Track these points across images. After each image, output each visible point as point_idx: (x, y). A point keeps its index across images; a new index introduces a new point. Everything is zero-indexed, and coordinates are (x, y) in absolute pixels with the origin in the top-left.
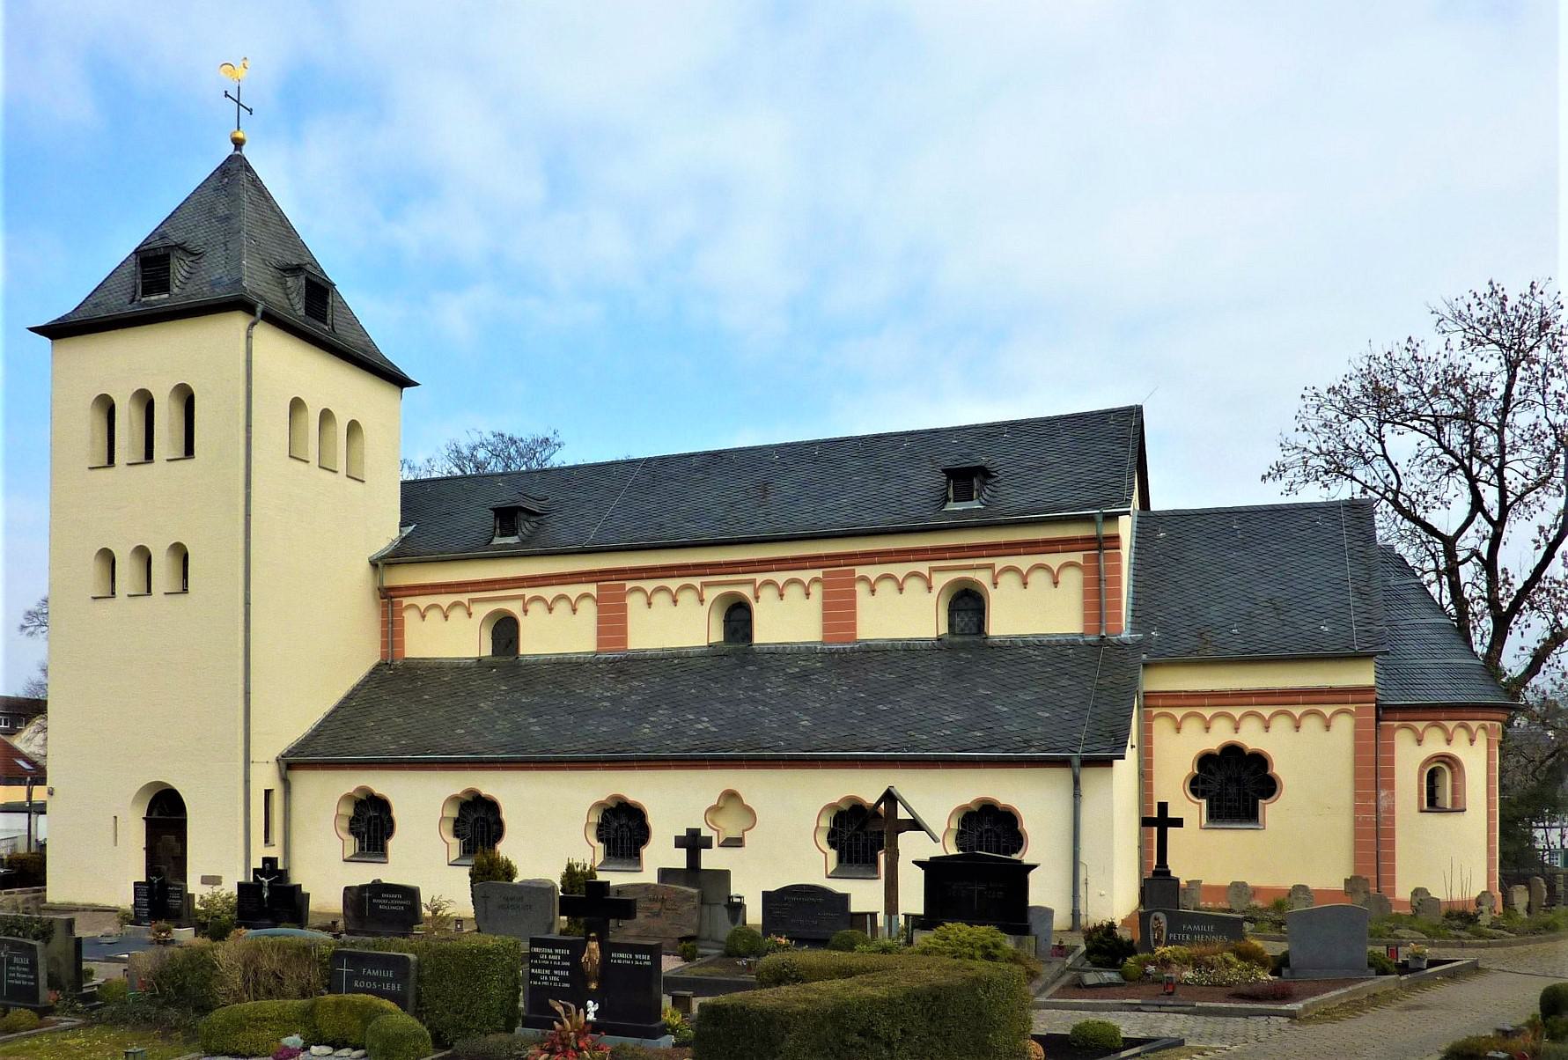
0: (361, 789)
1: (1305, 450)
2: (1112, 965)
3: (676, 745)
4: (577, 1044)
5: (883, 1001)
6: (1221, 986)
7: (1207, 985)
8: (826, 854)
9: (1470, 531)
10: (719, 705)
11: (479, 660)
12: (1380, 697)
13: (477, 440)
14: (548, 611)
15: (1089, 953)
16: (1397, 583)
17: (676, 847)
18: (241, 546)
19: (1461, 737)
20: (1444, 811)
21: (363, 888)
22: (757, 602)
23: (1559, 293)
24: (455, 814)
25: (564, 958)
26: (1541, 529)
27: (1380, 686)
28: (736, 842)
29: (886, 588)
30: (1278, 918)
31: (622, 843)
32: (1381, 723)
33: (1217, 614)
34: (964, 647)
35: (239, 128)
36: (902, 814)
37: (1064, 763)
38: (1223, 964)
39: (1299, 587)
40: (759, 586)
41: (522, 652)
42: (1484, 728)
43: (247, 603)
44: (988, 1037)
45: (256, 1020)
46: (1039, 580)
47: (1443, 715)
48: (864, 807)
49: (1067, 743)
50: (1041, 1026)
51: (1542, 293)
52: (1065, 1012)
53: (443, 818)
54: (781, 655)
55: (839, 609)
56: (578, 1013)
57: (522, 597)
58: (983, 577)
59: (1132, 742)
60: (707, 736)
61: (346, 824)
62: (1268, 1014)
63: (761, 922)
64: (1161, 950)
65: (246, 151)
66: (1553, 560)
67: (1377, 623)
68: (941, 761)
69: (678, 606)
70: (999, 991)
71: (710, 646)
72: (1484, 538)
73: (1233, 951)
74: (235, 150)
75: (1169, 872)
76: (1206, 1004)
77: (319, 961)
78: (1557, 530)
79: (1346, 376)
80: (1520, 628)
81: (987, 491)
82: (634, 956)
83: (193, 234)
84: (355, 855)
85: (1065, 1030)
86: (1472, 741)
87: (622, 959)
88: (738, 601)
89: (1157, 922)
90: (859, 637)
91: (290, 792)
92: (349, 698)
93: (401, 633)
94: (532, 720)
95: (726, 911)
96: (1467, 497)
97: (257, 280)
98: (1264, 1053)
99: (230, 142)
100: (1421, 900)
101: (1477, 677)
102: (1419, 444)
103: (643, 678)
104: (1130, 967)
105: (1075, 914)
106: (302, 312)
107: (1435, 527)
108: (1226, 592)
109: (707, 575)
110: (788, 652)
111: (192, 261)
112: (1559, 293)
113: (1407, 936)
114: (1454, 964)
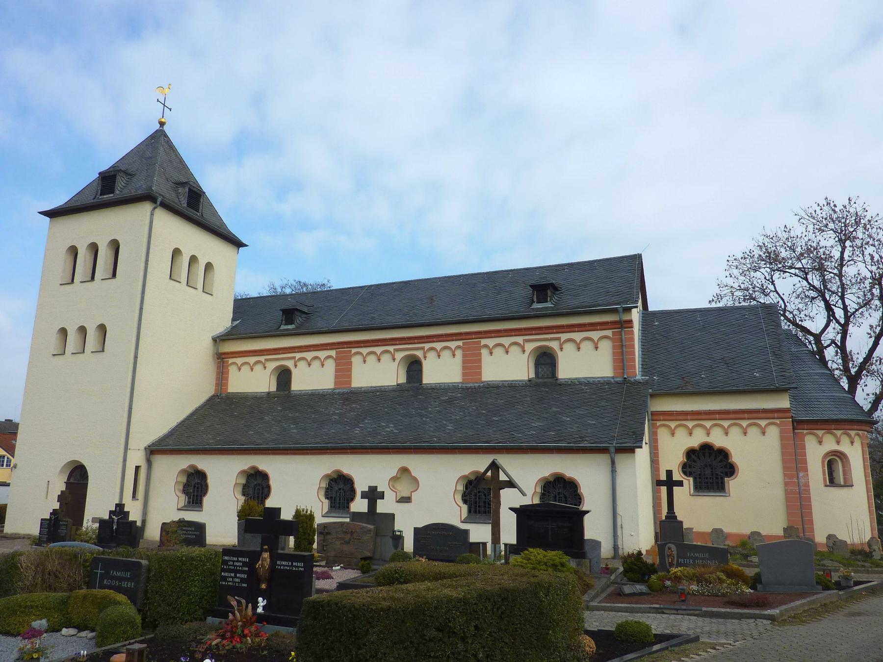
1: (732, 287)
2: (641, 581)
3: (373, 440)
4: (243, 631)
5: (459, 600)
6: (717, 596)
7: (708, 595)
8: (461, 507)
9: (830, 329)
10: (400, 418)
11: (269, 393)
12: (794, 415)
13: (285, 282)
15: (625, 572)
16: (796, 350)
17: (361, 498)
19: (845, 440)
20: (839, 486)
22: (425, 360)
23: (865, 203)
26: (871, 326)
27: (793, 409)
28: (406, 500)
29: (499, 351)
30: (745, 552)
31: (340, 500)
32: (796, 431)
34: (545, 385)
35: (163, 117)
36: (503, 477)
37: (604, 450)
38: (717, 580)
40: (427, 350)
42: (858, 435)
43: (136, 357)
44: (548, 634)
45: (25, 607)
46: (587, 346)
47: (833, 427)
49: (607, 439)
50: (594, 623)
51: (855, 203)
52: (611, 613)
53: (236, 484)
55: (472, 364)
56: (247, 607)
58: (554, 345)
59: (645, 440)
60: (392, 435)
61: (181, 487)
62: (755, 617)
63: (413, 551)
64: (674, 570)
65: (165, 128)
66: (879, 346)
67: (789, 371)
68: (529, 449)
69: (563, 352)
70: (557, 595)
71: (398, 385)
72: (838, 333)
73: (723, 571)
74: (160, 127)
75: (676, 517)
76: (710, 609)
77: (83, 565)
78: (880, 328)
80: (861, 387)
81: (556, 298)
82: (292, 564)
84: (185, 506)
85: (595, 628)
86: (852, 443)
87: (284, 566)
89: (670, 551)
91: (151, 468)
93: (227, 379)
94: (292, 426)
95: (391, 540)
96: (824, 313)
97: (160, 186)
98: (761, 648)
100: (835, 541)
102: (794, 285)
104: (654, 582)
105: (616, 548)
107: (808, 328)
108: (696, 355)
109: (397, 345)
110: (442, 388)
112: (865, 203)
113: (829, 565)
114: (869, 584)
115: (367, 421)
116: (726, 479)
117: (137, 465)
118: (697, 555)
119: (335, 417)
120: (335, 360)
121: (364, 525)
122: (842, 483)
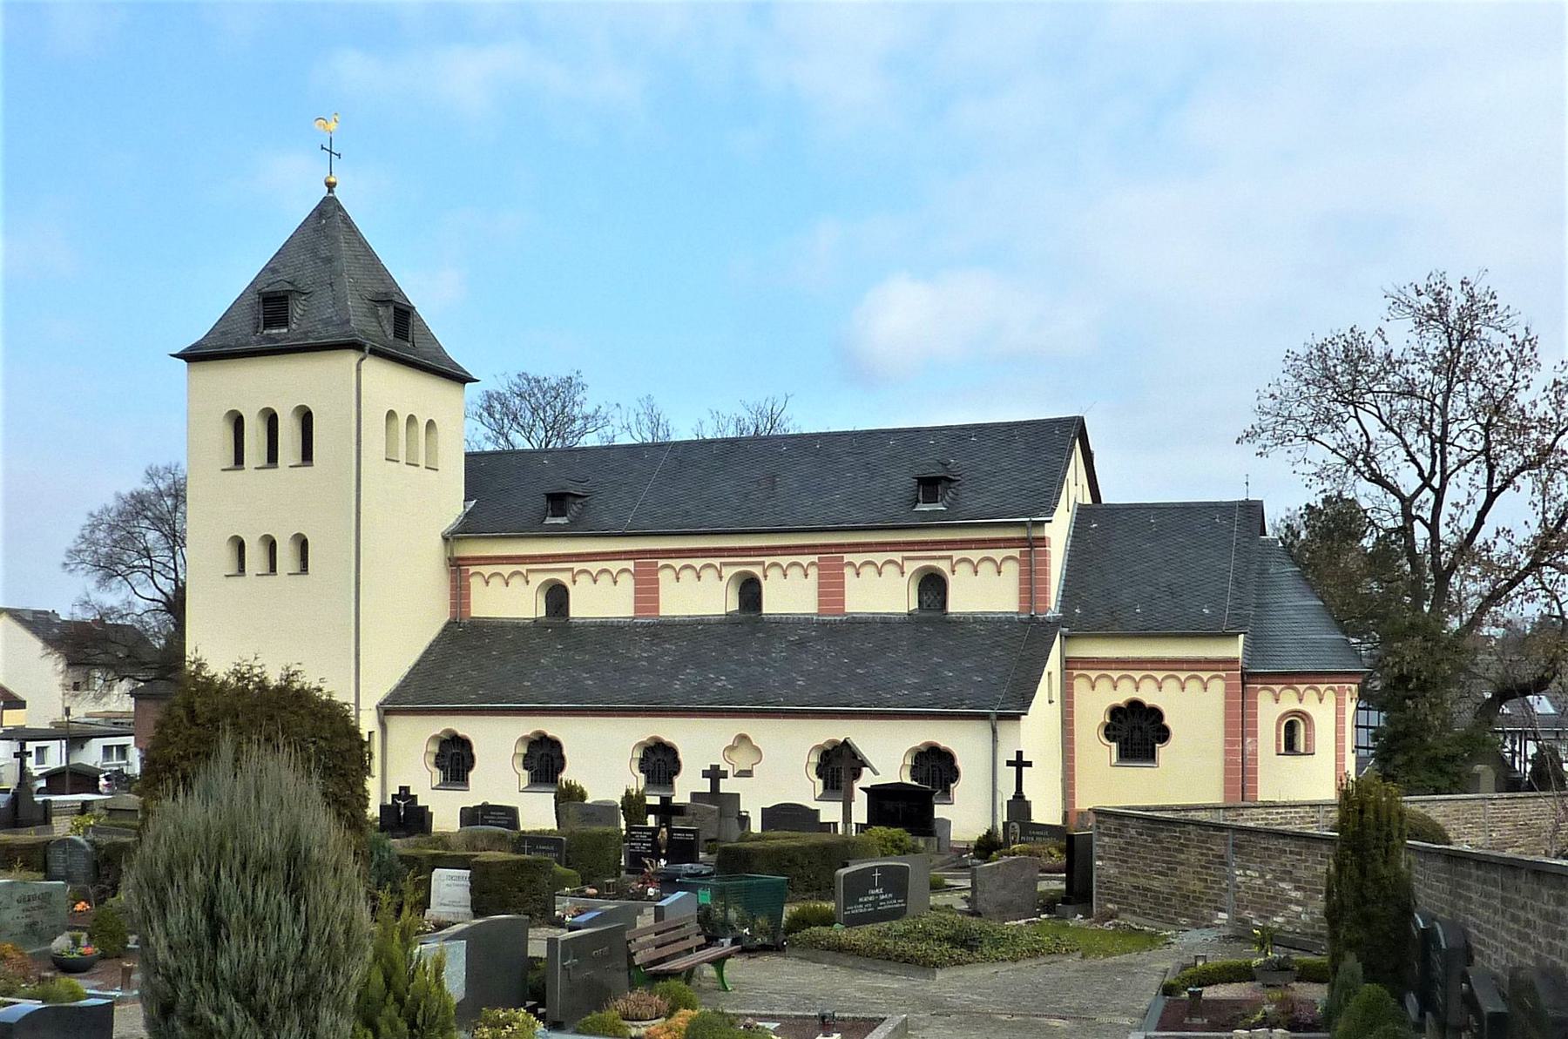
0: (447, 731)
5: (800, 847)
8: (814, 783)
10: (733, 667)
11: (536, 620)
17: (738, 795)
18: (353, 538)
19: (1311, 696)
21: (476, 808)
24: (525, 751)
25: (648, 837)
28: (747, 774)
29: (868, 572)
31: (659, 774)
33: (1126, 595)
34: (928, 621)
37: (984, 717)
39: (1193, 575)
41: (572, 614)
47: (1295, 680)
54: (785, 624)
55: (831, 588)
57: (572, 569)
58: (944, 566)
61: (433, 759)
66: (1483, 526)
74: (329, 192)
79: (1326, 339)
83: (301, 273)
84: (440, 785)
88: (750, 577)
90: (847, 610)
92: (428, 652)
94: (585, 675)
95: (737, 821)
97: (360, 321)
101: (1326, 649)
103: (674, 642)
106: (391, 337)
111: (305, 300)
115: (688, 671)
116: (1157, 745)
118: (1038, 833)
119: (644, 663)
120: (634, 575)
121: (708, 806)
122: (1302, 751)
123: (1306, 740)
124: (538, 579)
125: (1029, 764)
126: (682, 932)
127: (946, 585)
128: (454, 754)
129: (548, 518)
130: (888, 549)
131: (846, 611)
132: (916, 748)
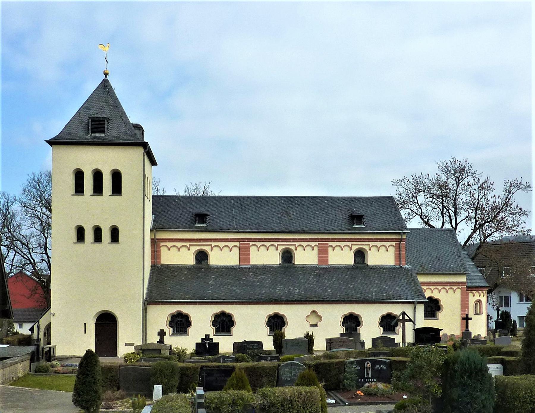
14: (220, 251)
28: (316, 326)
29: (338, 249)
46: (383, 249)
48: (182, 314)
55: (323, 255)
57: (211, 245)
65: (109, 78)
69: (190, 251)
74: (105, 77)
75: (469, 330)
95: (360, 344)
99: (103, 74)
117: (508, 308)
122: (479, 313)
123: (480, 309)
124: (194, 249)
125: (471, 319)
126: (198, 389)
127: (208, 257)
128: (178, 321)
129: (196, 224)
130: (224, 241)
131: (329, 264)
132: (216, 313)
